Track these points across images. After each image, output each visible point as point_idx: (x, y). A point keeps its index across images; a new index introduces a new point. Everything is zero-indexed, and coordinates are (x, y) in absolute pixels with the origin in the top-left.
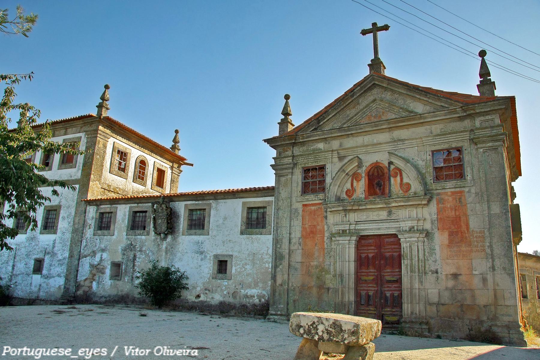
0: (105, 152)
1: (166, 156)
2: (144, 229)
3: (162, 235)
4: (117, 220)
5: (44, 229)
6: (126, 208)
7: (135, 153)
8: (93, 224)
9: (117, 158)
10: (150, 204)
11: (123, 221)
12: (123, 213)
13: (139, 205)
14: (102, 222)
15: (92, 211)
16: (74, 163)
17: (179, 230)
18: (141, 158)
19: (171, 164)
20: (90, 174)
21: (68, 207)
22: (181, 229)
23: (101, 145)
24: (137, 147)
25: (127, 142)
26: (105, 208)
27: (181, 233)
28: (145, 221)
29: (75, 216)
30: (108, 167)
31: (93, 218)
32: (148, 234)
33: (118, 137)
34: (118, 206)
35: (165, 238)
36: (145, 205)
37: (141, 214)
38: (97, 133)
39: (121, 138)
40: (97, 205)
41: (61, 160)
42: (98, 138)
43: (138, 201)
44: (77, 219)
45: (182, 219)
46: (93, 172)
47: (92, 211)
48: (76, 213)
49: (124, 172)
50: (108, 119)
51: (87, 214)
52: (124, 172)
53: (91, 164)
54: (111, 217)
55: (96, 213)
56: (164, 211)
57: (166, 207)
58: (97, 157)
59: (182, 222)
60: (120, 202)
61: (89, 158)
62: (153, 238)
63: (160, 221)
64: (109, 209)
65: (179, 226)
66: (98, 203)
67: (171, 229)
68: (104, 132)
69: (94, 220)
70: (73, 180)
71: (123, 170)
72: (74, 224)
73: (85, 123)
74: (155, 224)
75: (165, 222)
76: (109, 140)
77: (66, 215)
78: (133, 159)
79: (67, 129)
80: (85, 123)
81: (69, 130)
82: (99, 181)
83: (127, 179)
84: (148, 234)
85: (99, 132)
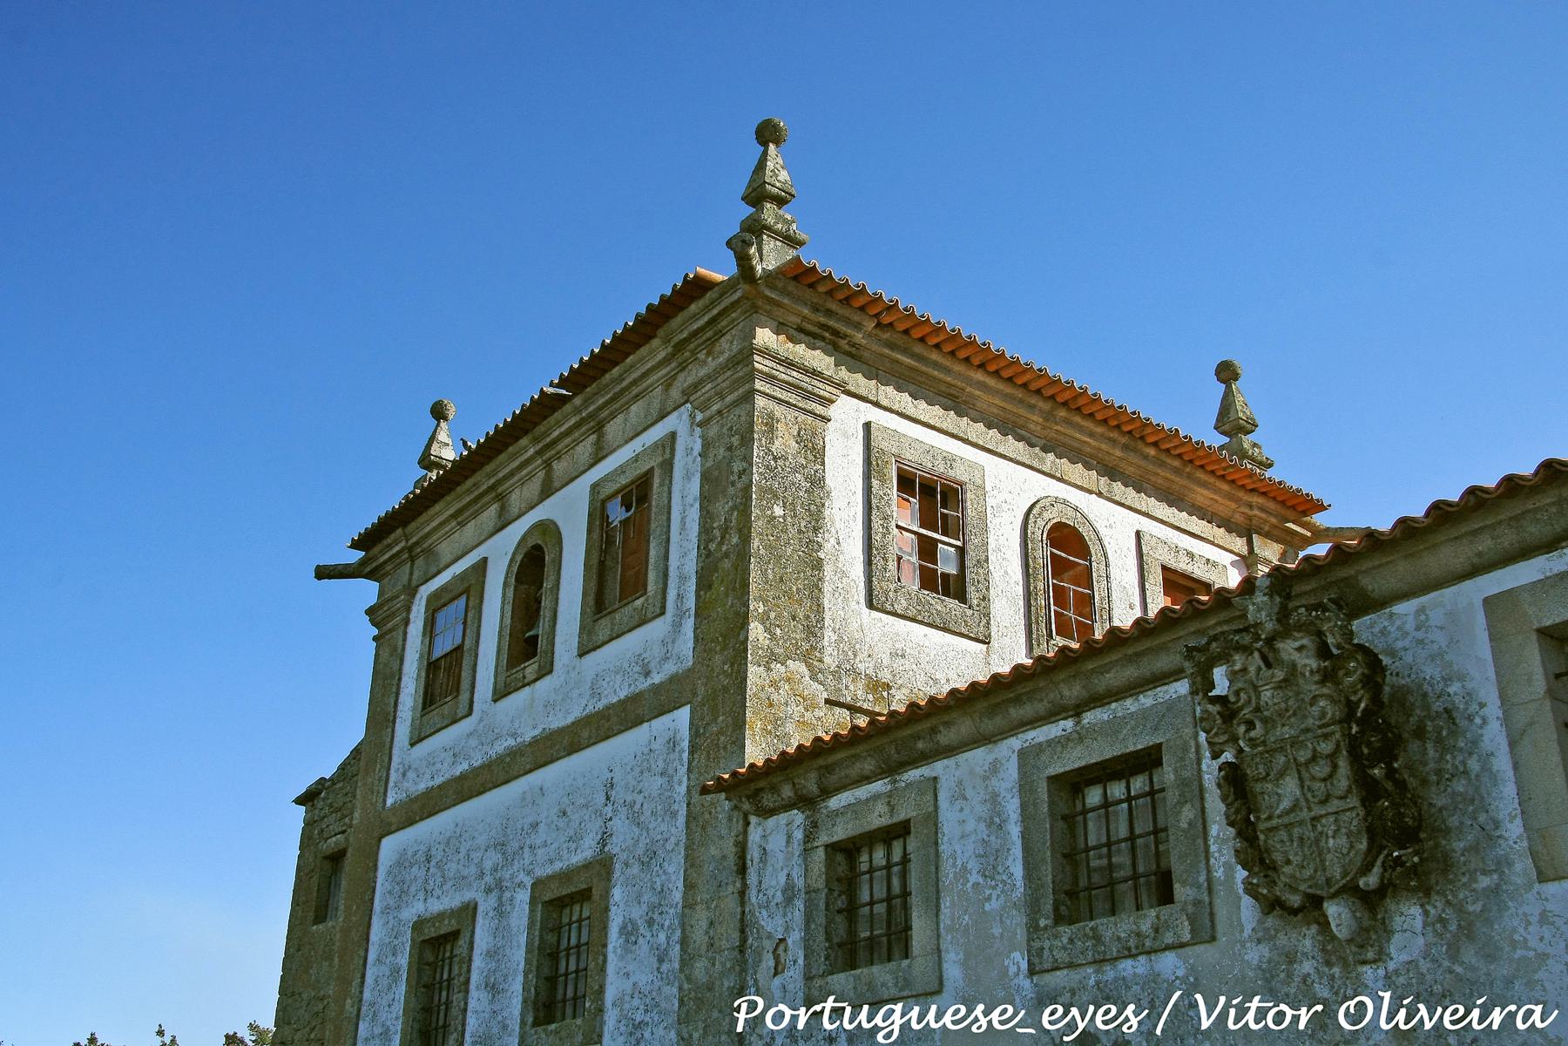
0: (817, 482)
1: (1202, 495)
2: (1165, 896)
3: (1332, 909)
4: (948, 872)
5: (536, 1024)
6: (995, 768)
7: (1010, 490)
8: (795, 937)
9: (903, 514)
10: (1182, 688)
11: (991, 863)
12: (979, 808)
13: (1089, 717)
14: (851, 911)
15: (780, 845)
16: (651, 588)
17: (1490, 835)
18: (1054, 516)
19: (1240, 544)
20: (742, 621)
21: (649, 859)
22: (1514, 830)
23: (785, 442)
24: (1012, 446)
25: (950, 420)
26: (859, 804)
27: (1522, 866)
28: (1158, 832)
29: (689, 905)
30: (857, 571)
31: (789, 893)
32: (1204, 932)
33: (888, 394)
34: (938, 768)
35: (1371, 937)
36: (1130, 705)
37: (1117, 790)
38: (751, 375)
39: (904, 401)
40: (805, 802)
41: (591, 600)
42: (760, 402)
43: (1072, 691)
44: (701, 918)
45: (1494, 736)
46: (756, 607)
47: (780, 845)
48: (689, 886)
49: (962, 597)
50: (800, 276)
51: (752, 878)
52: (962, 597)
53: (743, 555)
54: (905, 860)
55: (807, 851)
56: (1310, 687)
57: (1323, 651)
58: (768, 513)
59: (1502, 763)
60: (946, 737)
61: (725, 530)
62: (1255, 954)
63: (1290, 788)
64: (881, 807)
65: (1477, 801)
66: (811, 785)
67: (1408, 836)
68: (789, 364)
69: (799, 904)
70: (656, 689)
71: (955, 587)
72: (686, 961)
73: (680, 347)
74: (1246, 830)
75: (1343, 780)
76: (832, 411)
77: (637, 913)
78: (1006, 517)
79: (599, 428)
80: (680, 347)
81: (613, 429)
82: (810, 656)
83: (985, 641)
84: (1204, 932)
85: (760, 363)
